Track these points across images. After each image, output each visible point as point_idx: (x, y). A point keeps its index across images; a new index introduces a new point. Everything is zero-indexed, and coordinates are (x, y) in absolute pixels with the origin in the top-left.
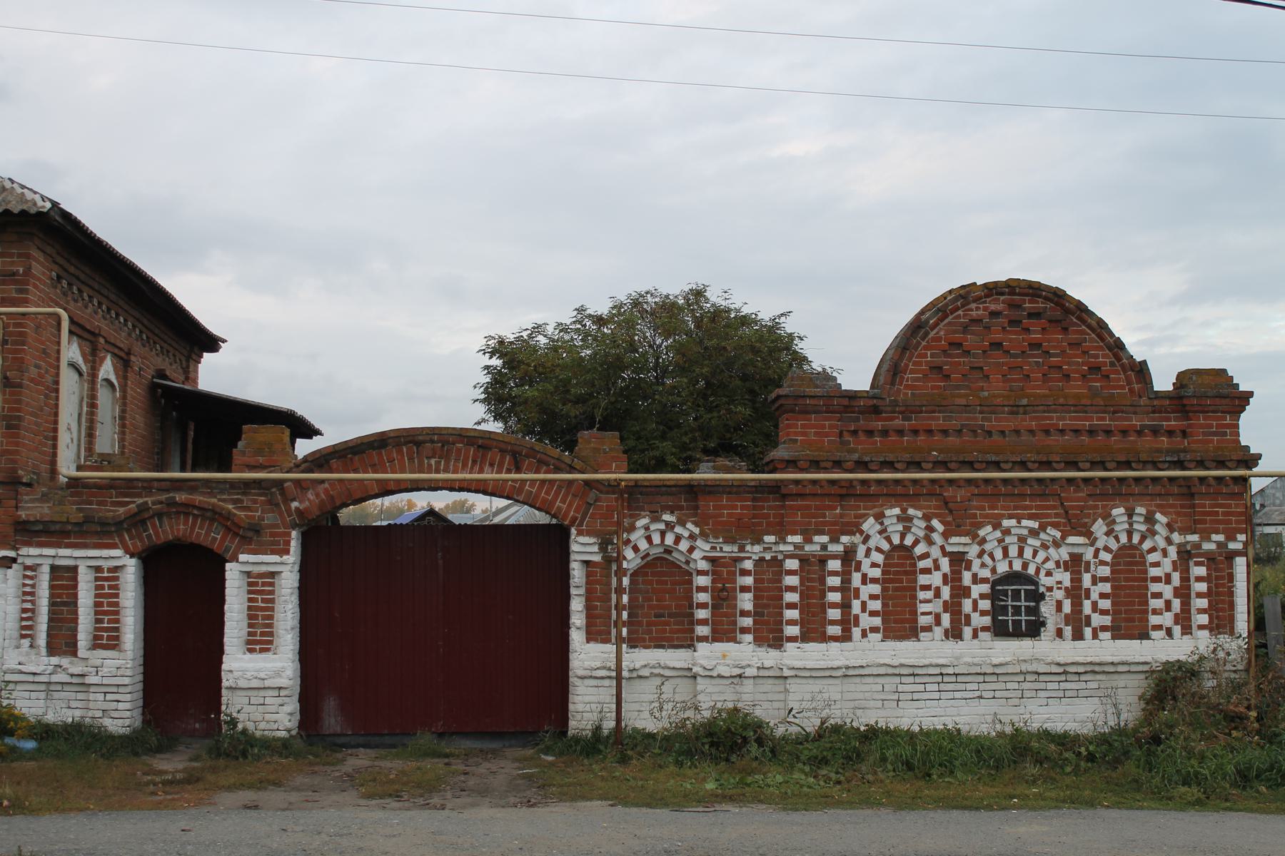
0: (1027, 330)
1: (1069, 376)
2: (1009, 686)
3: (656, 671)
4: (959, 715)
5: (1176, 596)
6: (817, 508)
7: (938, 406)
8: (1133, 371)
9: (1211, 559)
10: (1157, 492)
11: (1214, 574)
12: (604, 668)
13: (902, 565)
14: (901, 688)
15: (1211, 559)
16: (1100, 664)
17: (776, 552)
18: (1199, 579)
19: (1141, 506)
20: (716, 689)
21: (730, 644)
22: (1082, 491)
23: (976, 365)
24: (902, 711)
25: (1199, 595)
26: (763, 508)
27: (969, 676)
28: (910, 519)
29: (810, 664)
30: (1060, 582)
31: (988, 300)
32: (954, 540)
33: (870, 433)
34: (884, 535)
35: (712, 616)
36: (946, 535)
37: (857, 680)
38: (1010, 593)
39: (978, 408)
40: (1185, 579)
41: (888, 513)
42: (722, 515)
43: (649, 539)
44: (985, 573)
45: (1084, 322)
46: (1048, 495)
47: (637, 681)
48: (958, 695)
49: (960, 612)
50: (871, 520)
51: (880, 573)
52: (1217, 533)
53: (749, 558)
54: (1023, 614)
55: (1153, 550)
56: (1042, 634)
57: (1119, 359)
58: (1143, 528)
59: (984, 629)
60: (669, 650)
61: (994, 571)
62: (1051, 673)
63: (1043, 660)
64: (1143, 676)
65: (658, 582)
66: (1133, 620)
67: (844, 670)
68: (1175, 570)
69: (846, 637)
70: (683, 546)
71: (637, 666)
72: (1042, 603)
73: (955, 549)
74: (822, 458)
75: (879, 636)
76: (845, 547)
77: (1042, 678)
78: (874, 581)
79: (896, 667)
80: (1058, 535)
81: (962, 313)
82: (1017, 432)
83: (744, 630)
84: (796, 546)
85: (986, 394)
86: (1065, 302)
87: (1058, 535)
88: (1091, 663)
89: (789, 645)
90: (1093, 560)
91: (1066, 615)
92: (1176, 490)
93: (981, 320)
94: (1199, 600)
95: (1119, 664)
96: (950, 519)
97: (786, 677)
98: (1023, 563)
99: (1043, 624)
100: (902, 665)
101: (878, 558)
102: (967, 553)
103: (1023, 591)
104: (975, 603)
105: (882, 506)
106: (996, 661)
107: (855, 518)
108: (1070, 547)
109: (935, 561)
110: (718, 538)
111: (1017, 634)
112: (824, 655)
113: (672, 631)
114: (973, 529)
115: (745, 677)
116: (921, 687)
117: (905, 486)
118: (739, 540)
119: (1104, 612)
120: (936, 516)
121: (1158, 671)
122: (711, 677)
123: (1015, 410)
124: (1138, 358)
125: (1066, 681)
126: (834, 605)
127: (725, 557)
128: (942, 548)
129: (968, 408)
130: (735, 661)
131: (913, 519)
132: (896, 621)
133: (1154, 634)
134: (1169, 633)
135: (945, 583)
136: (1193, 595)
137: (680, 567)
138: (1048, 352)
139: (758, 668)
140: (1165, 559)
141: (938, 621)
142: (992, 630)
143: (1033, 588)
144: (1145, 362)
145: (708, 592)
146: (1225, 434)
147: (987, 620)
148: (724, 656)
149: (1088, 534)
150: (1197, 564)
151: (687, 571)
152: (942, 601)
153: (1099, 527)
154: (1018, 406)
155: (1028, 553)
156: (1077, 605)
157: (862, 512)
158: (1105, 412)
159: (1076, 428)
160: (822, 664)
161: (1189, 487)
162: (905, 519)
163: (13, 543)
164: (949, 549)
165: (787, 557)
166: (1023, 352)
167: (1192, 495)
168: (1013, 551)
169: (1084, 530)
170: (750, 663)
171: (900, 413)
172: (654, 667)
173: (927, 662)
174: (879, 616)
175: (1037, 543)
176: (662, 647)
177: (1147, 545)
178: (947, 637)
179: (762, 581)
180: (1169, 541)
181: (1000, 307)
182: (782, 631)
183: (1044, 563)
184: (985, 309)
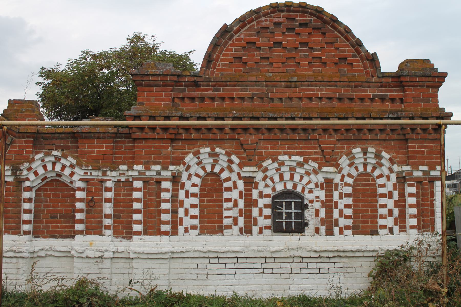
0: (298, 34)
1: (325, 63)
2: (283, 265)
3: (49, 253)
4: (248, 284)
5: (395, 206)
6: (155, 148)
7: (238, 82)
8: (368, 60)
9: (419, 182)
10: (384, 138)
11: (421, 192)
12: (12, 251)
13: (213, 185)
15: (419, 182)
16: (343, 251)
17: (128, 176)
18: (411, 195)
19: (373, 147)
20: (85, 266)
21: (96, 236)
22: (334, 137)
23: (264, 56)
24: (210, 281)
25: (411, 206)
26: (121, 148)
27: (256, 259)
28: (217, 155)
30: (318, 197)
31: (273, 15)
32: (246, 169)
33: (192, 99)
35: (86, 218)
36: (241, 166)
37: (181, 260)
38: (284, 204)
39: (264, 83)
40: (402, 195)
41: (202, 151)
42: (93, 152)
43: (45, 167)
44: (268, 191)
45: (336, 29)
46: (311, 140)
48: (248, 271)
49: (251, 216)
50: (191, 155)
52: (423, 165)
53: (110, 180)
54: (293, 218)
55: (381, 176)
56: (306, 231)
57: (359, 53)
58: (374, 161)
59: (267, 228)
60: (59, 239)
61: (274, 189)
62: (310, 257)
63: (305, 249)
64: (373, 259)
65: (54, 196)
66: (367, 222)
67: (170, 254)
68: (395, 189)
69: (175, 232)
70: (67, 172)
71: (36, 250)
72: (306, 211)
74: (157, 115)
75: (197, 232)
76: (172, 173)
77: (305, 260)
78: (194, 195)
79: (205, 252)
80: (316, 166)
81: (256, 23)
82: (291, 99)
83: (108, 227)
84: (140, 172)
85: (271, 74)
86: (323, 16)
87: (316, 166)
88: (337, 251)
89: (135, 237)
90: (340, 183)
91: (322, 219)
92: (396, 137)
93: (268, 28)
94: (411, 210)
95: (356, 251)
96: (244, 155)
97: (132, 258)
98: (294, 184)
99: (307, 224)
100: (210, 251)
101: (197, 181)
102: (255, 177)
103: (293, 203)
104: (261, 210)
105: (200, 146)
106: (273, 249)
107: (182, 154)
108: (325, 174)
109: (234, 183)
110: (88, 166)
111: (289, 230)
112: (157, 244)
113: (62, 227)
114: (260, 162)
115: (104, 258)
117: (214, 134)
118: (102, 167)
119: (347, 217)
120: (235, 153)
121: (382, 256)
122: (82, 257)
123: (289, 84)
124: (371, 52)
125: (321, 262)
127: (94, 179)
128: (239, 174)
129: (257, 83)
130: (98, 247)
131: (219, 155)
132: (209, 222)
133: (381, 231)
134: (391, 230)
135: (241, 197)
136: (407, 206)
138: (312, 48)
139: (114, 252)
140: (388, 182)
141: (236, 223)
142: (272, 228)
143: (300, 201)
144: (375, 54)
145: (84, 202)
146: (429, 101)
147: (269, 222)
148: (91, 244)
149: (337, 165)
150: (410, 185)
152: (238, 209)
153: (344, 161)
154: (291, 82)
155: (297, 178)
156: (329, 212)
157: (187, 150)
158: (349, 86)
159: (329, 96)
160: (155, 250)
161: (404, 135)
162: (213, 155)
163: (167, 53)
164: (243, 175)
165: (135, 179)
166: (296, 48)
167: (406, 140)
168: (287, 176)
169: (334, 163)
170: (107, 249)
171: (212, 86)
172: (47, 250)
173: (226, 249)
175: (303, 171)
176: (55, 237)
177: (376, 173)
178: (241, 233)
179: (119, 195)
180: (391, 170)
181: (280, 20)
182: (131, 228)
183: (307, 184)
184: (271, 21)
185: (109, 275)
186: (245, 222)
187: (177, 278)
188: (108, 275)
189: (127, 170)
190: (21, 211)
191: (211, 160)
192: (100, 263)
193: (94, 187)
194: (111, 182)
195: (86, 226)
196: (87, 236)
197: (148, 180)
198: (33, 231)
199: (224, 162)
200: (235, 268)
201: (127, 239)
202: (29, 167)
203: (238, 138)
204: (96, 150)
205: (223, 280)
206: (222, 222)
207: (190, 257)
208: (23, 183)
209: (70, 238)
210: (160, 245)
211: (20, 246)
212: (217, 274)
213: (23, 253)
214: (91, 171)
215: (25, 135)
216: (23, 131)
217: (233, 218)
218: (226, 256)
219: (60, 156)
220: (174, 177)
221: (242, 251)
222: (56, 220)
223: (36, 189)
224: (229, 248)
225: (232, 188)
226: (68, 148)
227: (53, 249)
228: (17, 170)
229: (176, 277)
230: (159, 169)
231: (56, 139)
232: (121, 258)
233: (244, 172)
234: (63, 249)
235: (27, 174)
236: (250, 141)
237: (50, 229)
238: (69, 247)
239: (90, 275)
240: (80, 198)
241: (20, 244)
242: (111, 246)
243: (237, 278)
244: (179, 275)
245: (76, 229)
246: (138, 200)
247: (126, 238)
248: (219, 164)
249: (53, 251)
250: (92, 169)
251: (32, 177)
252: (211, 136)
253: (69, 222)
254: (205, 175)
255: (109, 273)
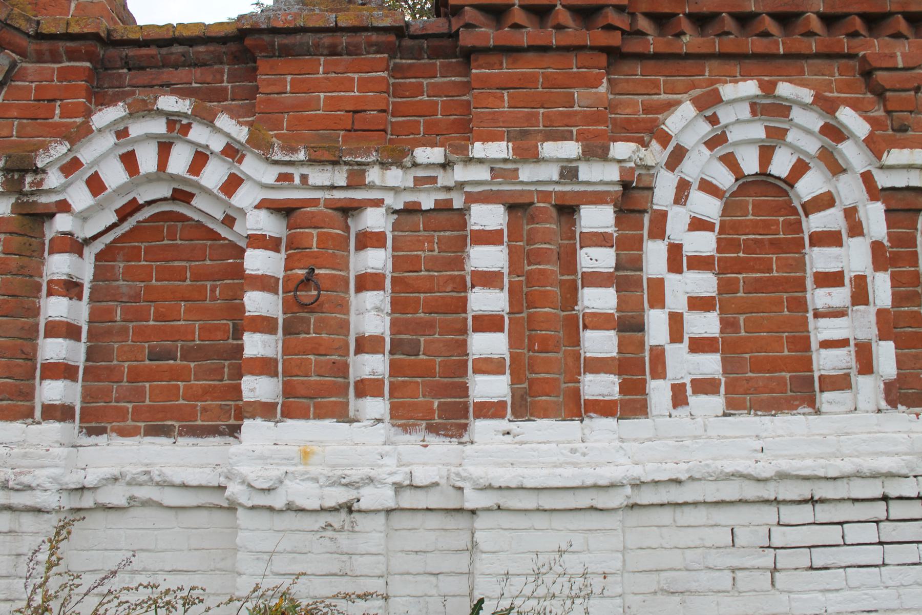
6: (551, 84)
13: (766, 227)
14: (780, 537)
17: (448, 189)
24: (785, 597)
28: (782, 109)
29: (536, 476)
32: (896, 156)
34: (721, 151)
35: (284, 353)
37: (666, 516)
43: (129, 161)
47: (100, 516)
50: (687, 110)
51: (714, 245)
53: (378, 203)
60: (181, 440)
67: (628, 490)
71: (91, 480)
73: (899, 180)
75: (717, 402)
76: (622, 170)
78: (699, 263)
79: (766, 480)
83: (366, 388)
84: (497, 169)
89: (481, 427)
97: (473, 512)
100: (782, 476)
105: (713, 83)
107: (645, 111)
109: (851, 213)
110: (294, 150)
112: (574, 451)
113: (192, 395)
115: (359, 511)
116: (833, 534)
120: (855, 106)
122: (271, 509)
126: (599, 321)
127: (315, 202)
128: (867, 178)
130: (334, 467)
131: (790, 108)
132: (757, 366)
137: (216, 236)
139: (398, 488)
141: (866, 365)
148: (306, 455)
151: (233, 245)
157: (663, 97)
160: (568, 476)
164: (884, 180)
165: (472, 198)
170: (372, 473)
173: (846, 466)
174: (715, 351)
178: (892, 402)
182: (464, 390)
185: (382, 582)
186: (898, 362)
187: (654, 587)
188: (376, 580)
189: (446, 166)
190: (37, 331)
191: (758, 131)
192: (342, 530)
193: (315, 232)
194: (382, 210)
195: (285, 384)
196: (290, 422)
197: (527, 201)
198: (82, 408)
199: (809, 137)
200: (881, 543)
201: (446, 436)
202: (68, 159)
203: (851, 52)
204: (322, 95)
205: (837, 590)
206: (807, 364)
207: (705, 503)
208: (46, 225)
209: (222, 434)
210: (584, 455)
211: (25, 462)
212: (811, 568)
213: (38, 493)
214: (305, 170)
215: (62, 46)
216: (53, 30)
217: (852, 348)
218: (845, 495)
219: (185, 115)
220: (626, 185)
221: (904, 471)
222: (171, 366)
223: (98, 250)
224: (856, 460)
225: (839, 232)
226: (219, 95)
227: (157, 479)
228: (24, 171)
229: (650, 582)
230: (574, 155)
231: (176, 66)
232: (428, 509)
233: (887, 172)
234: (194, 477)
235: (64, 188)
236: (899, 59)
237: (147, 402)
238: (219, 470)
239: (302, 579)
240: (260, 273)
241: (25, 456)
242: (386, 460)
243: (890, 583)
244: (663, 574)
245: (247, 396)
246: (488, 279)
247: (445, 429)
248: (790, 145)
249: (158, 484)
250: (312, 162)
251: (80, 198)
252: (753, 44)
253: (217, 373)
254: (735, 189)
255: (378, 572)
